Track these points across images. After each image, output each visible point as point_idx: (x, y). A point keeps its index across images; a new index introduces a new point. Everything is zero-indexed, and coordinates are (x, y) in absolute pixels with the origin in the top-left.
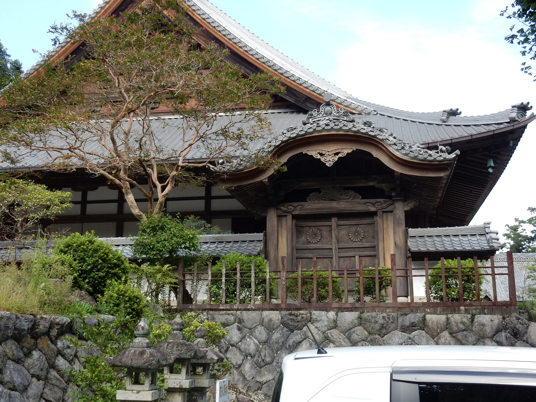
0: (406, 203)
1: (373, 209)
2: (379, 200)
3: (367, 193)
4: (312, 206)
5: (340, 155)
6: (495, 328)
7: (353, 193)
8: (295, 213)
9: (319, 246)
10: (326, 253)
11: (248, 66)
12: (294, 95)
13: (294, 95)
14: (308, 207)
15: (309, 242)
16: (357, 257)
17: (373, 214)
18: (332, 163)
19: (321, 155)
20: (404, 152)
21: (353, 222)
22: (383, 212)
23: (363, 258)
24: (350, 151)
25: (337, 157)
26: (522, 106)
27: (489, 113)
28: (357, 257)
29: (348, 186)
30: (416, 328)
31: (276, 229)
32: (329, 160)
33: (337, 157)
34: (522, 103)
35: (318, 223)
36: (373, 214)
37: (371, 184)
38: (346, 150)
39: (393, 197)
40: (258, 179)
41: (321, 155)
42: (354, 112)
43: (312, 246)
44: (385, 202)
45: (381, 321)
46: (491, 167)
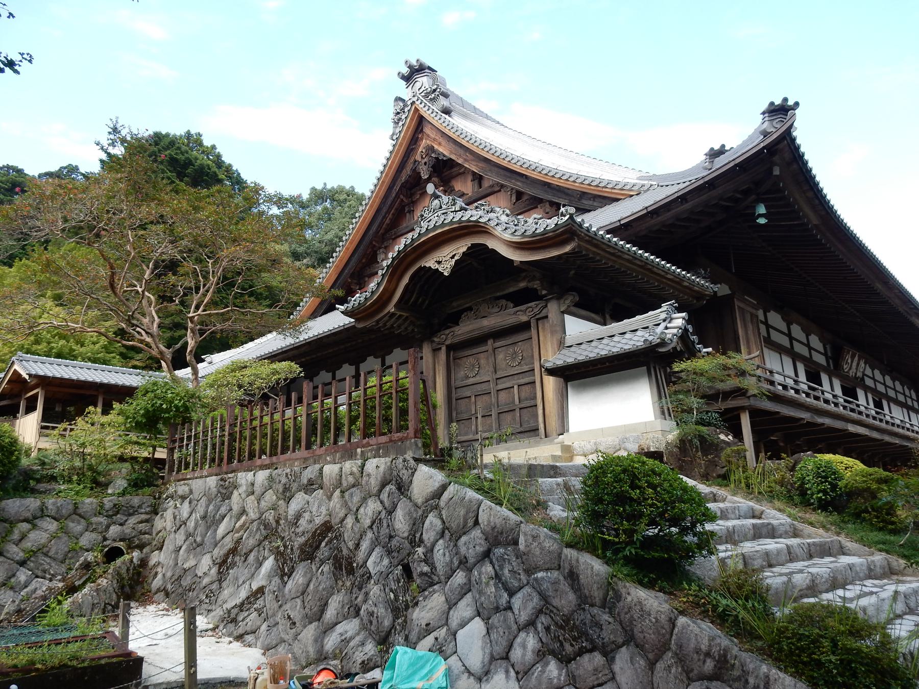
0: (562, 301)
1: (524, 318)
2: (530, 305)
3: (520, 298)
4: (465, 329)
5: (456, 258)
6: (379, 479)
7: (504, 302)
8: (448, 342)
9: (477, 379)
10: (484, 386)
11: (518, 178)
12: (567, 194)
13: (567, 194)
14: (460, 332)
15: (467, 377)
16: (516, 387)
17: (525, 327)
18: (449, 270)
19: (439, 263)
20: (510, 231)
21: (509, 341)
22: (538, 320)
23: (523, 387)
24: (464, 249)
25: (454, 260)
26: (772, 108)
27: (746, 137)
28: (516, 387)
29: (498, 294)
30: (314, 487)
31: (431, 366)
32: (446, 269)
33: (454, 260)
34: (772, 104)
35: (475, 351)
36: (525, 327)
37: (522, 285)
38: (460, 248)
39: (545, 296)
40: (386, 311)
41: (439, 263)
42: (632, 193)
43: (471, 381)
44: (537, 305)
45: (284, 480)
46: (761, 216)
